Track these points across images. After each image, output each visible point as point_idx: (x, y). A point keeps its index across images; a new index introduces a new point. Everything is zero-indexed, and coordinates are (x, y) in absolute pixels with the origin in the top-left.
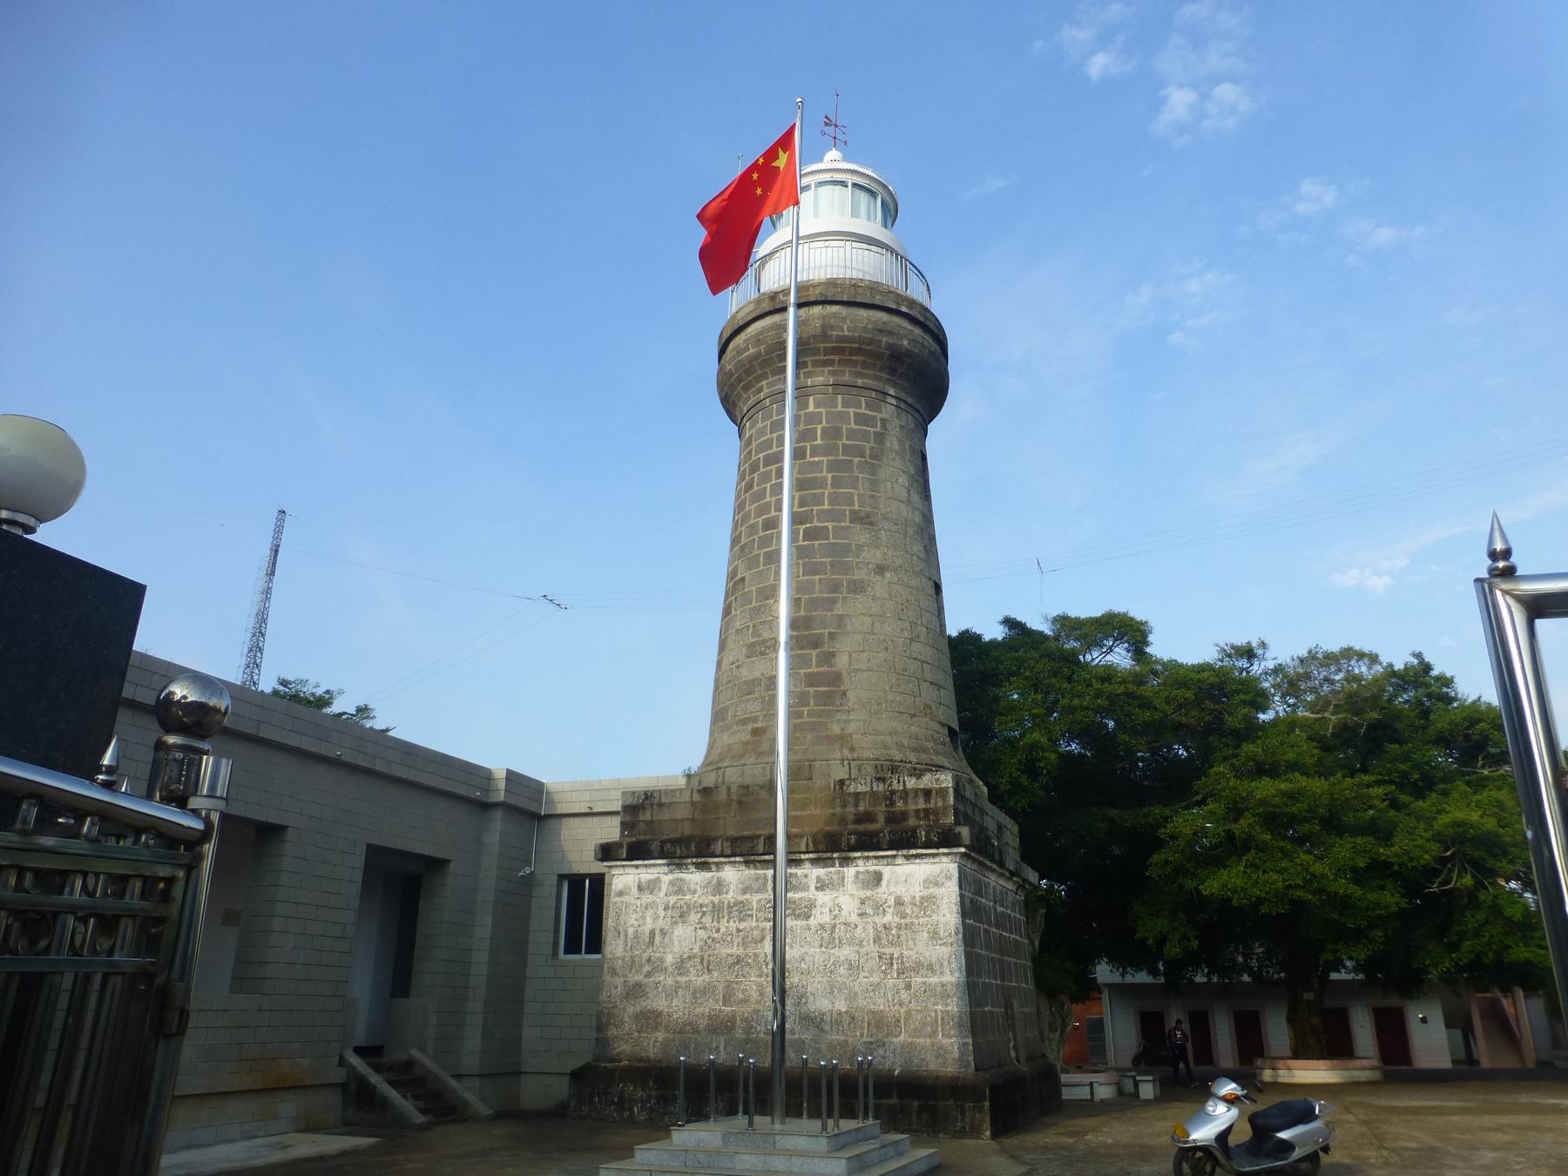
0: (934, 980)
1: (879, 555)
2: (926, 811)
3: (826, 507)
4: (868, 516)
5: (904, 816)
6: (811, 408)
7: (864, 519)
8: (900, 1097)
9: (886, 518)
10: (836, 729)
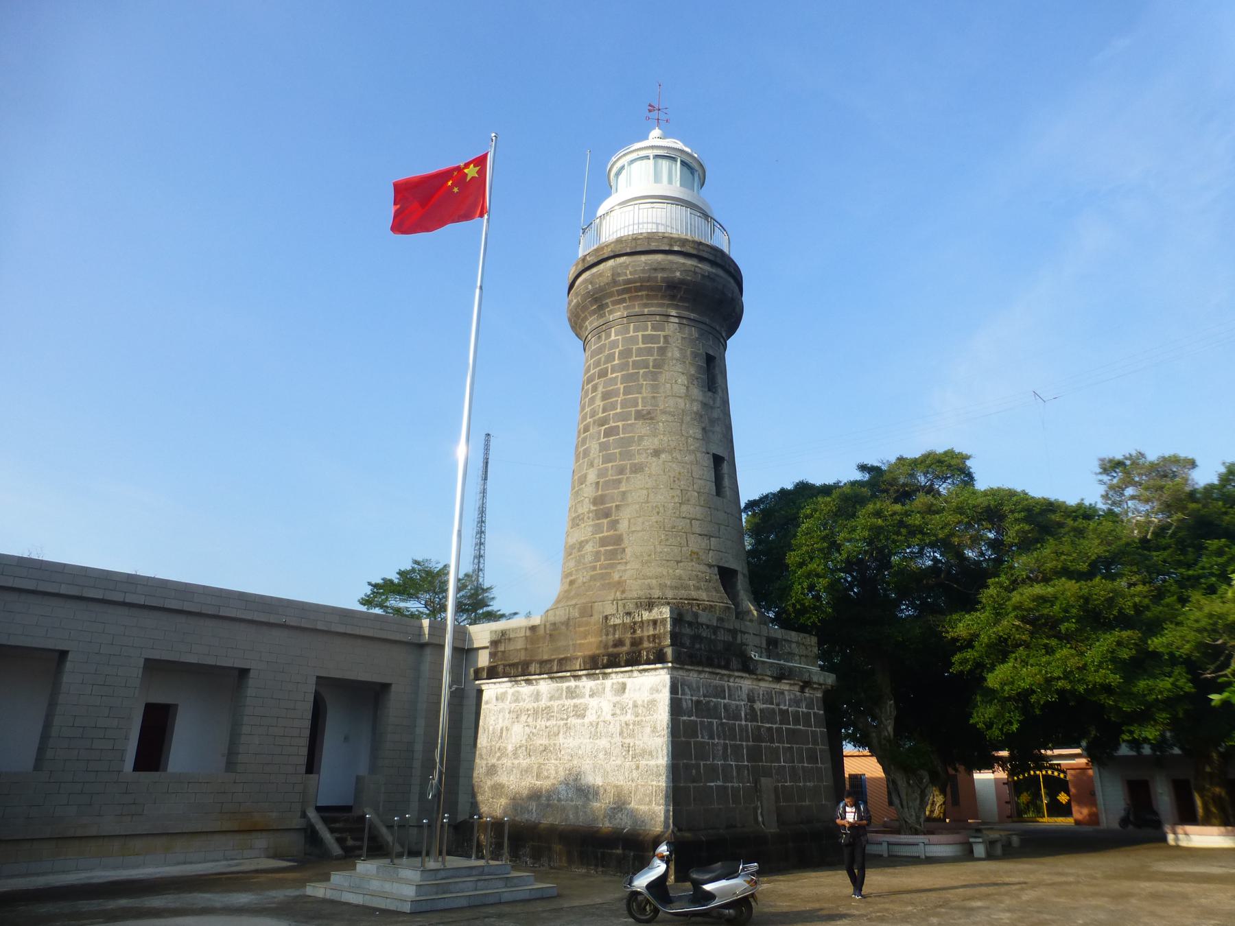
0: (652, 763)
1: (656, 441)
2: (654, 636)
4: (649, 413)
5: (641, 639)
6: (613, 338)
7: (645, 416)
8: (624, 849)
9: (664, 412)
10: (616, 577)
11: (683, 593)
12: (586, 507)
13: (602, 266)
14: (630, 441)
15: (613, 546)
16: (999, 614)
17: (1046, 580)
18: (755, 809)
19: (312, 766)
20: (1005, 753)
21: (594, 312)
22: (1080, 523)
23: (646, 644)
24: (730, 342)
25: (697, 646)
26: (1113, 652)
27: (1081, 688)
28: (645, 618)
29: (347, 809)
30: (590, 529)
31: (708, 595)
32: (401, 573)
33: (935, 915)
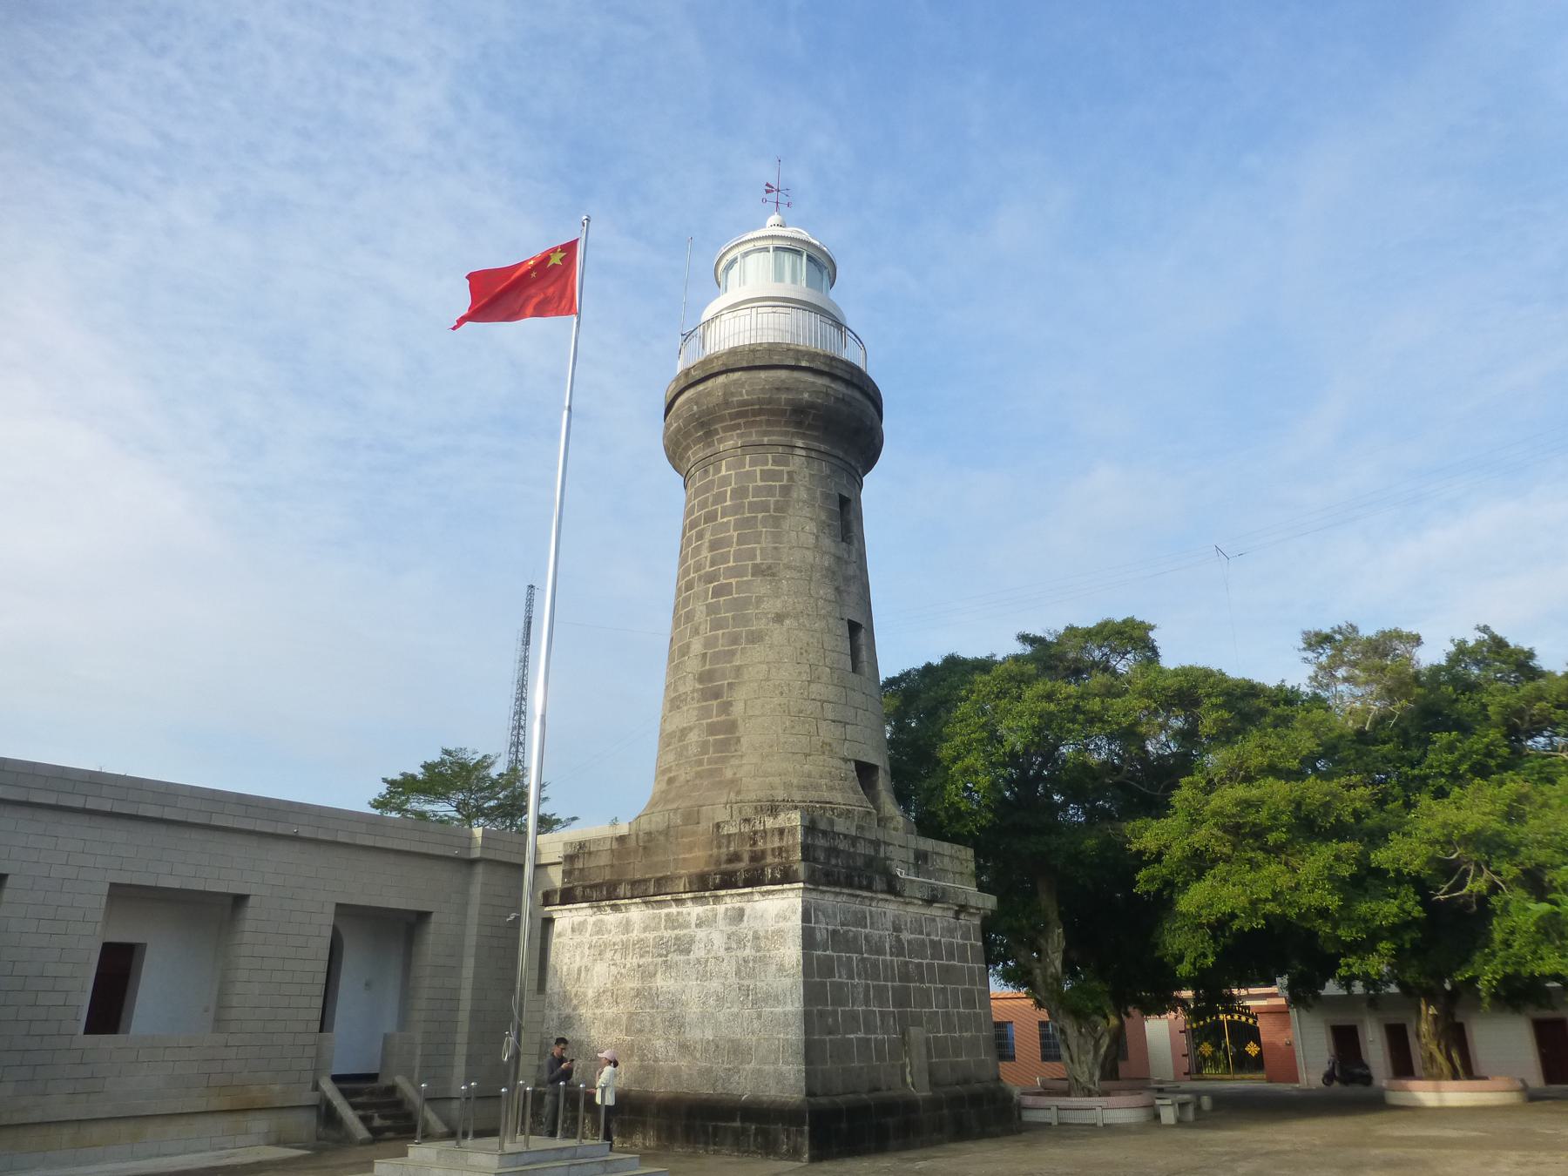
0: (779, 1010)
1: (779, 604)
2: (780, 849)
3: (731, 564)
4: (769, 568)
5: (763, 852)
6: (723, 472)
8: (743, 1120)
9: (789, 567)
10: (729, 774)
11: (813, 795)
12: (689, 686)
13: (710, 383)
14: (745, 603)
15: (725, 735)
16: (1195, 821)
17: (1248, 779)
18: (903, 1067)
19: (325, 1024)
20: (1187, 994)
21: (699, 440)
22: (1282, 710)
23: (769, 859)
25: (833, 861)
26: (1331, 868)
27: (1292, 913)
29: (373, 1077)
31: (845, 796)
32: (426, 766)
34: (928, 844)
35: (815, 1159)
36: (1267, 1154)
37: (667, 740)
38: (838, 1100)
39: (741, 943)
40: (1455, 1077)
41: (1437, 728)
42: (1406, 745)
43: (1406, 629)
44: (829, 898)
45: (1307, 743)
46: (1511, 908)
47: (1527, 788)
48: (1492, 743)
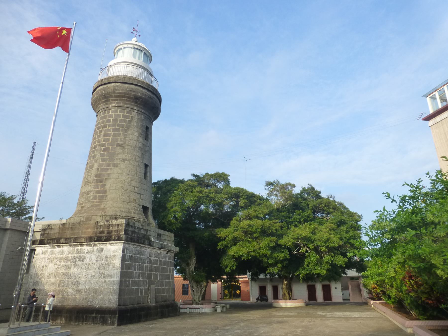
0: (112, 279)
1: (124, 156)
2: (117, 230)
3: (110, 142)
4: (122, 145)
5: (112, 231)
6: (110, 113)
8: (96, 314)
9: (128, 145)
10: (102, 206)
11: (129, 215)
12: (92, 178)
13: (109, 85)
14: (114, 154)
15: (102, 194)
16: (236, 229)
17: (250, 219)
18: (148, 297)
21: (104, 102)
23: (113, 233)
24: (155, 122)
25: (133, 235)
27: (258, 255)
28: (114, 223)
30: (93, 187)
31: (138, 216)
33: (217, 332)
34: (161, 232)
35: (118, 325)
36: (247, 320)
37: (82, 194)
38: (127, 307)
39: (101, 259)
40: (290, 299)
41: (296, 209)
42: (289, 213)
43: (292, 183)
44: (131, 246)
45: (266, 211)
46: (311, 256)
47: (317, 226)
48: (309, 214)
